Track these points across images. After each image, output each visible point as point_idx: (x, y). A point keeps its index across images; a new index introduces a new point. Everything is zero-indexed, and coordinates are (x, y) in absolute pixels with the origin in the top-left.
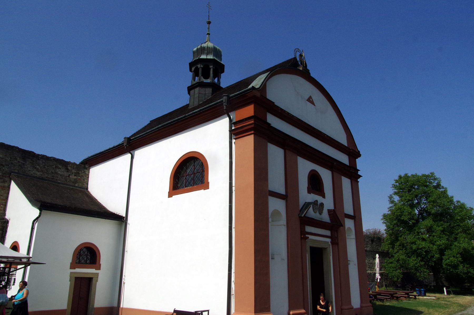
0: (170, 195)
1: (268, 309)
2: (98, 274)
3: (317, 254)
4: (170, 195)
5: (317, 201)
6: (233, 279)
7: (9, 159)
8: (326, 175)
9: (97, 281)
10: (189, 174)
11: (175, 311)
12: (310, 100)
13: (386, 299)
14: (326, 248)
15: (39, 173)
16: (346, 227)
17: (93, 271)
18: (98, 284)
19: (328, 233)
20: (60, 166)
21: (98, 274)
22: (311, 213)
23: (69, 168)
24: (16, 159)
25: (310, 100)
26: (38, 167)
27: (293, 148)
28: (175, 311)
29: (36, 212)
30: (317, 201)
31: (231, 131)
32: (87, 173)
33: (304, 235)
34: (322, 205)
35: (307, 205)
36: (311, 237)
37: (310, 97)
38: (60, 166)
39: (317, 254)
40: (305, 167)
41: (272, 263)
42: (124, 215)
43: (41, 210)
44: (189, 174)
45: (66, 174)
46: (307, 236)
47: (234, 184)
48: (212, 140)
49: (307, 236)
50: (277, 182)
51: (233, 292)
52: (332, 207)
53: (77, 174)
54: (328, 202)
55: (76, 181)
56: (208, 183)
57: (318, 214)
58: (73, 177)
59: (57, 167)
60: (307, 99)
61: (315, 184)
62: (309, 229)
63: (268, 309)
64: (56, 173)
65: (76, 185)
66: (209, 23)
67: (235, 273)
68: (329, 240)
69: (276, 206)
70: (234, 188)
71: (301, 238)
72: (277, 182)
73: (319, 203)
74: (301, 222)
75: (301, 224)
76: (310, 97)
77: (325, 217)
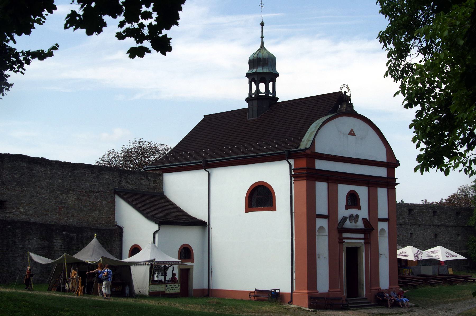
0: (247, 211)
1: (132, 56)
2: (193, 266)
3: (353, 253)
4: (247, 211)
5: (353, 214)
6: (294, 270)
7: (111, 179)
8: (362, 192)
9: (193, 271)
10: (260, 197)
11: (256, 290)
12: (352, 133)
13: (438, 283)
14: (360, 247)
15: (130, 186)
16: (379, 229)
17: (189, 264)
18: (194, 273)
19: (362, 236)
20: (143, 177)
21: (193, 266)
22: (348, 224)
23: (149, 177)
24: (116, 178)
25: (352, 133)
26: (129, 181)
27: (334, 179)
28: (256, 290)
29: (155, 227)
30: (353, 214)
31: (291, 176)
32: (161, 179)
33: (341, 241)
34: (357, 216)
35: (344, 219)
36: (346, 241)
37: (352, 130)
38: (143, 177)
39: (353, 253)
40: (343, 190)
41: (318, 261)
42: (206, 220)
43: (159, 226)
44: (260, 197)
45: (147, 183)
46: (344, 240)
47: (294, 211)
48: (277, 175)
49: (344, 240)
50: (322, 207)
51: (294, 278)
52: (367, 217)
53: (155, 182)
54: (363, 213)
55: (154, 188)
56: (276, 207)
57: (353, 223)
58: (152, 185)
59: (141, 179)
60: (348, 133)
61: (353, 200)
62: (345, 235)
63: (132, 56)
64: (141, 184)
65: (155, 191)
66: (262, 24)
67: (295, 267)
68: (362, 241)
69: (322, 223)
70: (294, 214)
71: (339, 243)
72: (322, 207)
73: (354, 216)
74: (339, 230)
75: (339, 233)
76: (352, 130)
77: (360, 224)
